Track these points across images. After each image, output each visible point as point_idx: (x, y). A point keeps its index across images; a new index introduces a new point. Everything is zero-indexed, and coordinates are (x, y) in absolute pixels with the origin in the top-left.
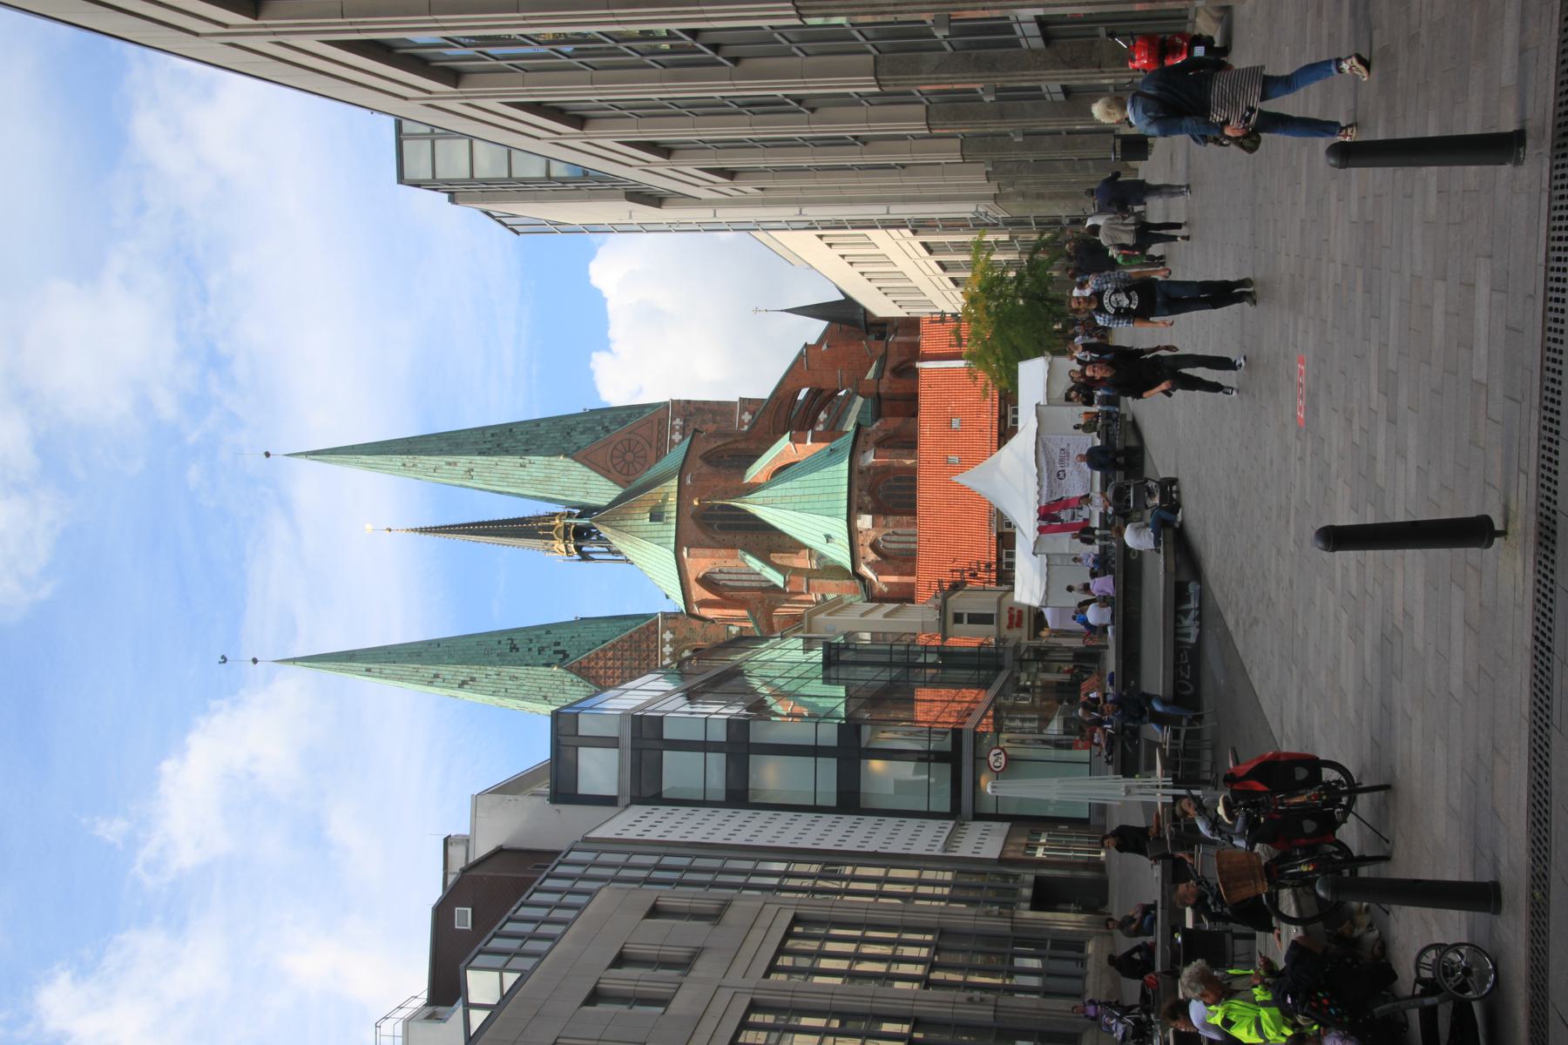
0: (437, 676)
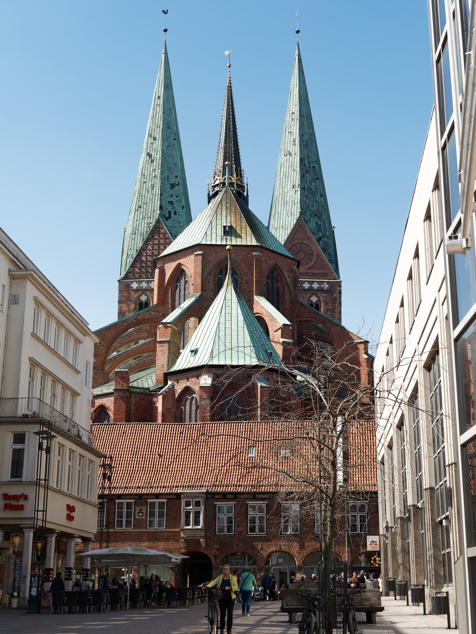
0: (155, 139)
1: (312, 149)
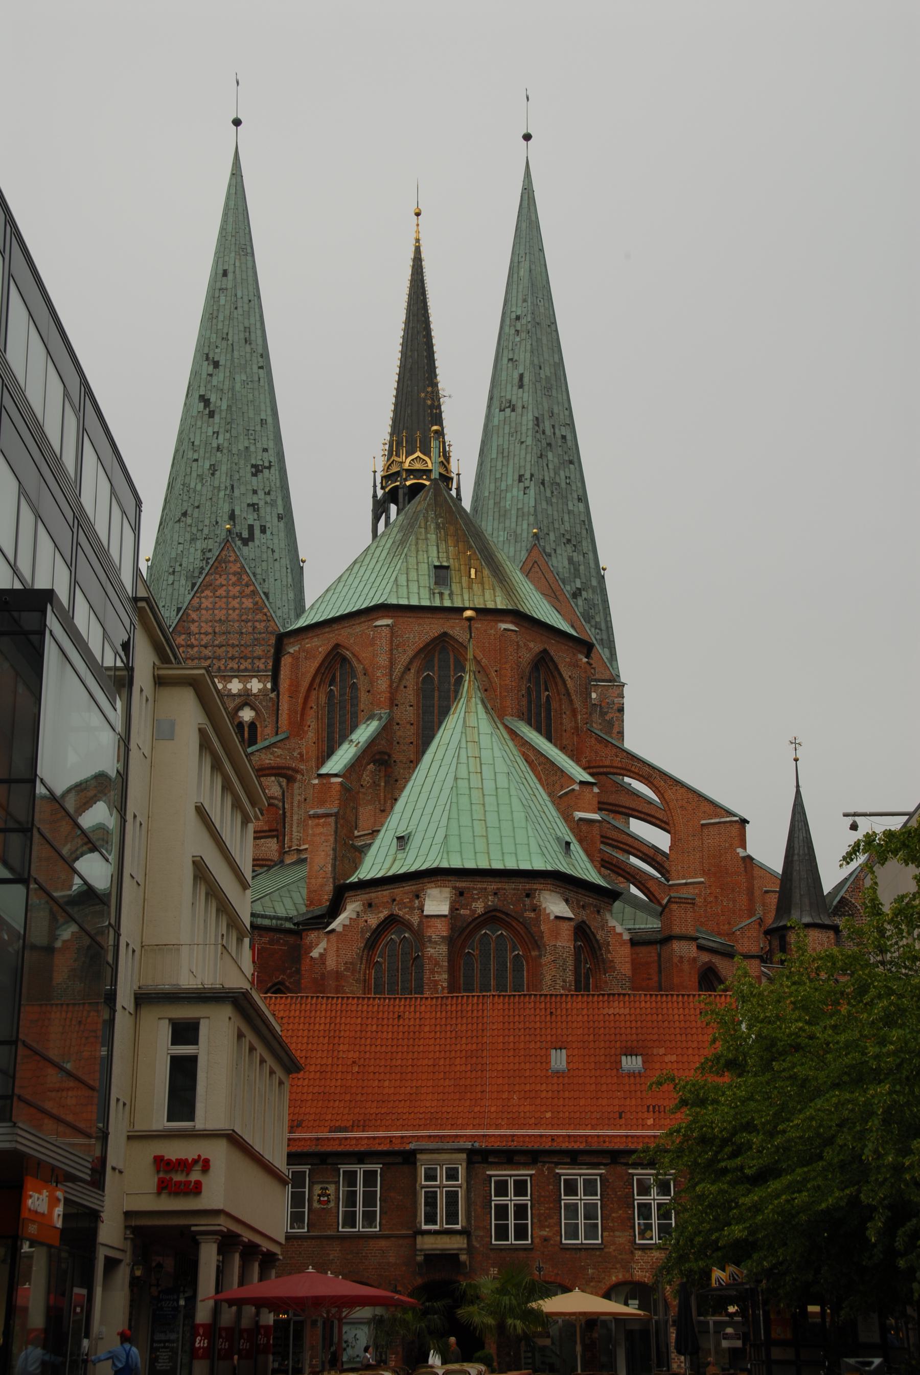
0: (216, 365)
1: (560, 396)
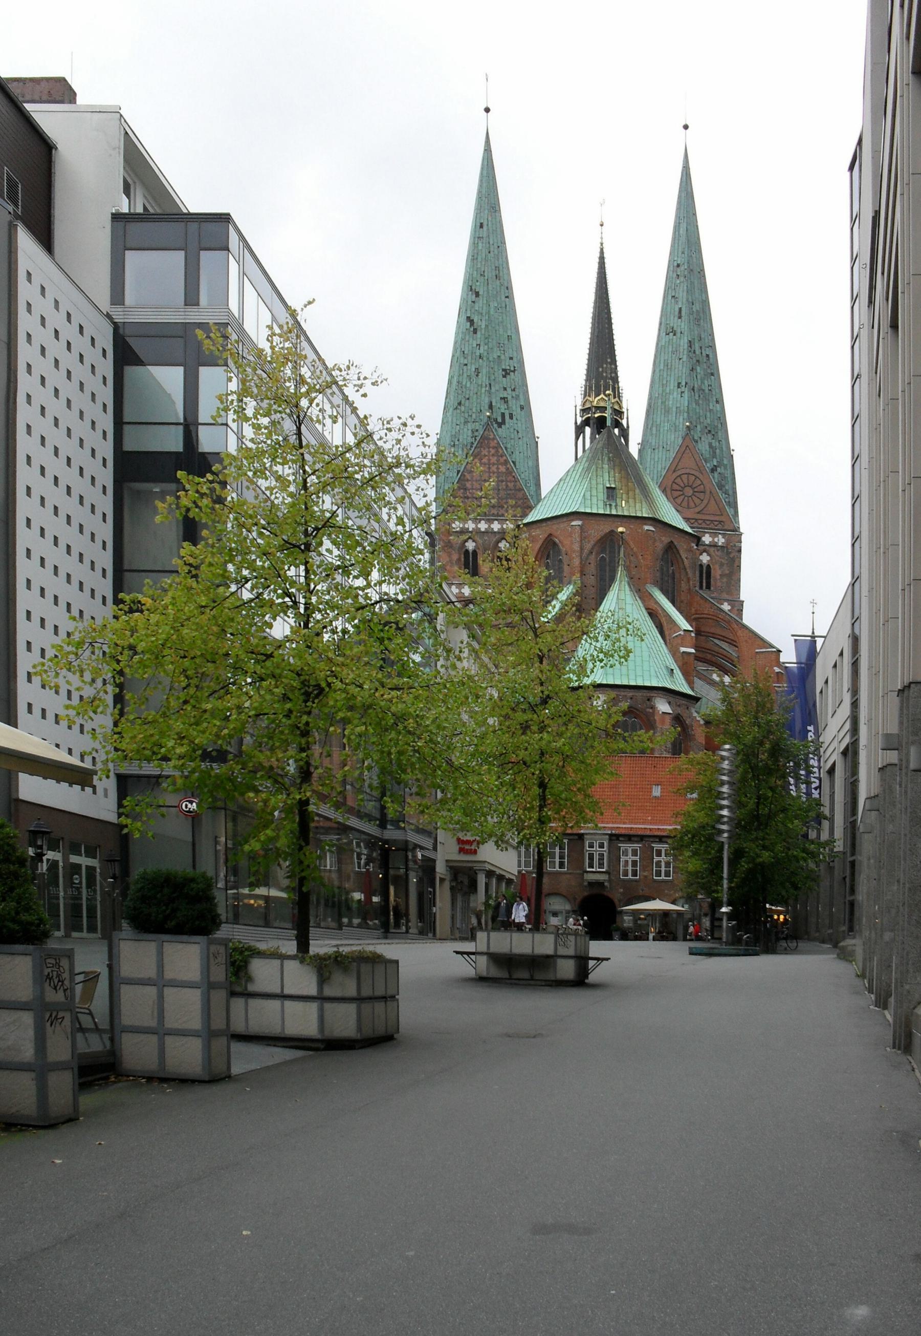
0: (477, 294)
